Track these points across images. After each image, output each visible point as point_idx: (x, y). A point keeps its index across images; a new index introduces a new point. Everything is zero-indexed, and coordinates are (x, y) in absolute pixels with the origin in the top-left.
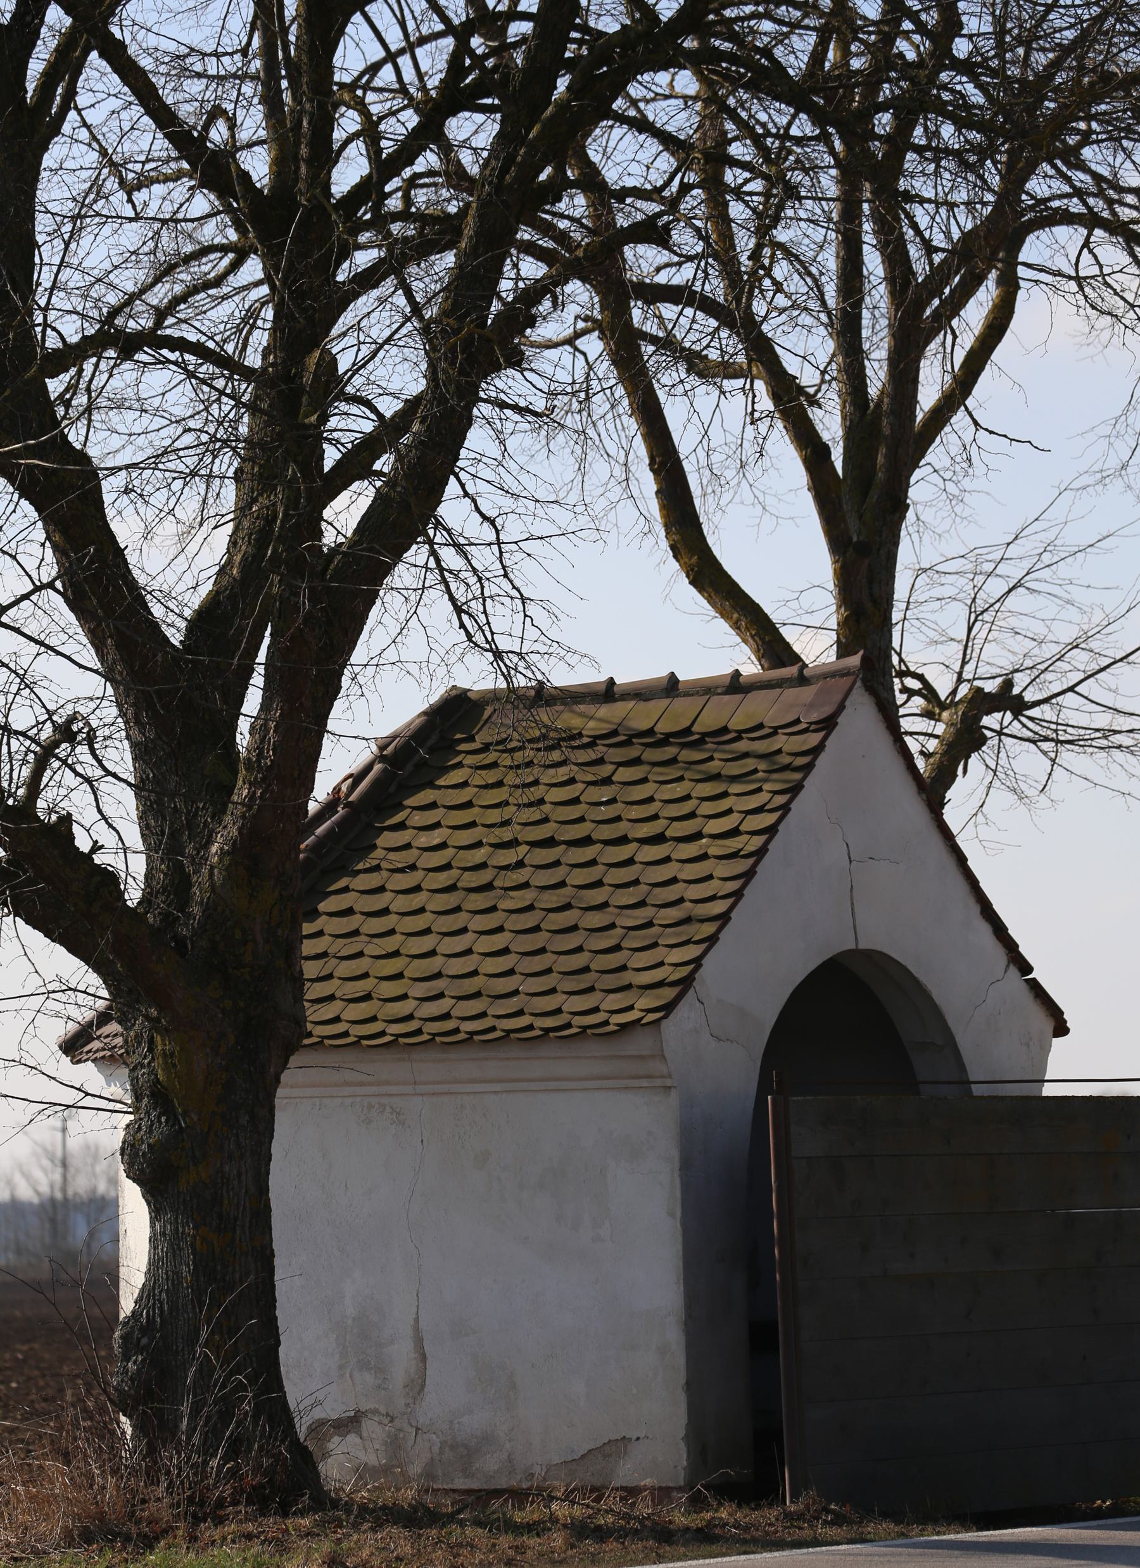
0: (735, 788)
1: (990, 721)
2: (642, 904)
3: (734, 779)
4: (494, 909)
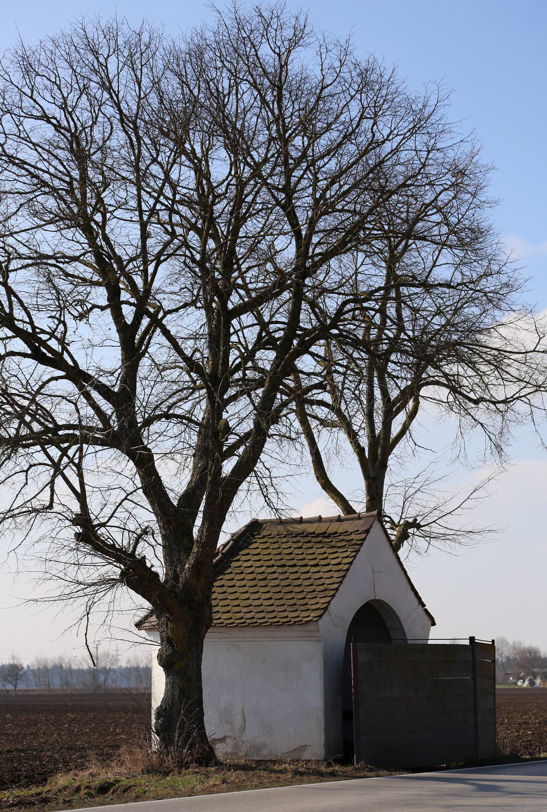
0: (340, 550)
1: (410, 531)
2: (312, 585)
3: (339, 547)
4: (267, 586)
